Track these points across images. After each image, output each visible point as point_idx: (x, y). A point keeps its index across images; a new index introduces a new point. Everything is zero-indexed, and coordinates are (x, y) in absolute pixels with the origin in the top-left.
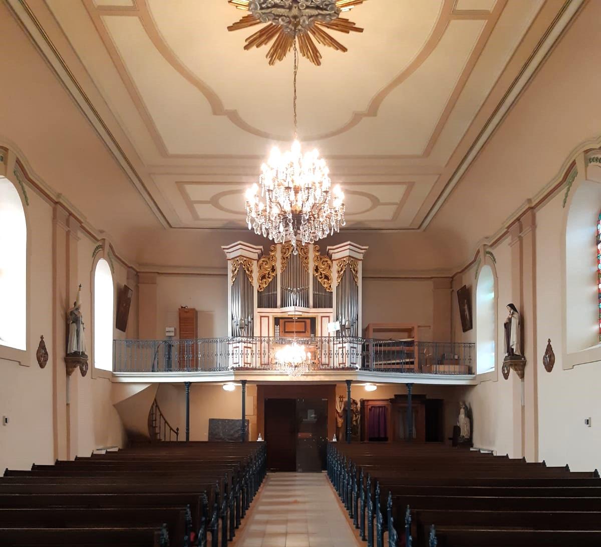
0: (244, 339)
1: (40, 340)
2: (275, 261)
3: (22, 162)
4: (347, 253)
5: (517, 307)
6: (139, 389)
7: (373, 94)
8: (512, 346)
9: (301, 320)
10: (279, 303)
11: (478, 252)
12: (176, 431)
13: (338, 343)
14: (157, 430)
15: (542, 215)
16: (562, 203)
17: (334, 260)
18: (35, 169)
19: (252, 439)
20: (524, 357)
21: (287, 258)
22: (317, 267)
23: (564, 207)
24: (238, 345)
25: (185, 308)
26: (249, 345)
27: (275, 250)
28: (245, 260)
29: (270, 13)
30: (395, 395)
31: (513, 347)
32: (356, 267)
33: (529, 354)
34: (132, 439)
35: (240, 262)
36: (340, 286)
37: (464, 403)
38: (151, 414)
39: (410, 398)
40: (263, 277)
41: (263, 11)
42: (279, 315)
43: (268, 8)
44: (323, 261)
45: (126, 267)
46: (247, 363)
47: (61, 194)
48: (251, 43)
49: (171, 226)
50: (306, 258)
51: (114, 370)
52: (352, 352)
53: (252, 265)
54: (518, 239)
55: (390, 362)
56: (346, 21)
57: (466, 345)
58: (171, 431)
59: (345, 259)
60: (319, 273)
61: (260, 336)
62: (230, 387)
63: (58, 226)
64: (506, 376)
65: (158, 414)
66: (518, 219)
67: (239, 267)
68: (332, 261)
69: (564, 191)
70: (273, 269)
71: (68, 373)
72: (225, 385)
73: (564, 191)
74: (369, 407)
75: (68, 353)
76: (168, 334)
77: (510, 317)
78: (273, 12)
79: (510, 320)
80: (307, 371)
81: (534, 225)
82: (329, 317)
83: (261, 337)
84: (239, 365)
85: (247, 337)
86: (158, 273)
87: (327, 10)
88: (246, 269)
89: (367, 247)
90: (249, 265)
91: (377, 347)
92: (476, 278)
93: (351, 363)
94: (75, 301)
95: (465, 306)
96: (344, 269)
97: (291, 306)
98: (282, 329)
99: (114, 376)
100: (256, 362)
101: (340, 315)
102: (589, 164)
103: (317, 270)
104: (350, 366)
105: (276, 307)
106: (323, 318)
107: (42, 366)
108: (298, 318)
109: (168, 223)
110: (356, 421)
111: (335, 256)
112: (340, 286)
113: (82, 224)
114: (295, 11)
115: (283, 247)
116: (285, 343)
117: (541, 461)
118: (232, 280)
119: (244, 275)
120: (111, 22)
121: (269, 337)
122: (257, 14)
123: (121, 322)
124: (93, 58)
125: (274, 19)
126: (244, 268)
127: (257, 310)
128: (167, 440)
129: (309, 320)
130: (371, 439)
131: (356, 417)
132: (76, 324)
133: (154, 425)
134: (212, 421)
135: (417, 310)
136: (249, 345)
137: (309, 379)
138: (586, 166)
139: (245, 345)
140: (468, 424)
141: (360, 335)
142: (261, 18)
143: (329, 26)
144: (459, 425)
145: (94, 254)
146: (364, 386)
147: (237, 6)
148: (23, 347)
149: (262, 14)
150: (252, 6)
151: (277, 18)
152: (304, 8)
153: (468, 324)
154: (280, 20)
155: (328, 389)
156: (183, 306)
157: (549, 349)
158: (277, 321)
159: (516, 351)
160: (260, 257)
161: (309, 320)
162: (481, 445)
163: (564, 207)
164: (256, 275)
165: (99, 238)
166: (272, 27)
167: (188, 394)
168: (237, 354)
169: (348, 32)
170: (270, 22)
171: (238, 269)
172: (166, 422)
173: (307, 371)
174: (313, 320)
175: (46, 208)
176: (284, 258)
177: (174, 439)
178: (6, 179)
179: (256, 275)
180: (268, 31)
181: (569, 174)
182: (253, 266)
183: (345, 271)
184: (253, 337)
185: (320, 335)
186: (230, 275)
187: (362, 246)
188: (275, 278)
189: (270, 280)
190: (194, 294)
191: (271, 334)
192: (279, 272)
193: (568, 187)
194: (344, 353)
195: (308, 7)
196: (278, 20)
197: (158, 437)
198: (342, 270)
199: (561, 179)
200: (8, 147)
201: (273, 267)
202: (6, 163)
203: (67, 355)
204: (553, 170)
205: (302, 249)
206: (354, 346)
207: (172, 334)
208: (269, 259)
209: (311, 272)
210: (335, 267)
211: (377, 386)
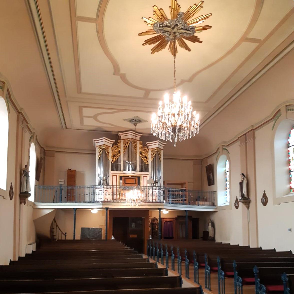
0: (105, 186)
1: (10, 185)
2: (120, 148)
3: (10, 91)
4: (157, 146)
5: (245, 174)
6: (48, 212)
7: (194, 72)
8: (244, 193)
9: (133, 177)
10: (122, 169)
11: (219, 148)
12: (65, 234)
13: (110, 188)
14: (54, 234)
15: (257, 133)
16: (272, 128)
17: (150, 149)
18: (15, 95)
19: (103, 238)
20: (249, 199)
21: (127, 147)
22: (141, 152)
23: (272, 130)
24: (102, 189)
25: (71, 169)
26: (107, 190)
27: (120, 143)
28: (106, 147)
29: (163, 29)
30: (178, 216)
31: (244, 194)
32: (108, 150)
33: (252, 197)
35: (103, 148)
36: (153, 162)
37: (211, 220)
38: (52, 225)
39: (187, 217)
40: (114, 156)
41: (159, 28)
42: (122, 175)
43: (163, 27)
44: (144, 149)
45: (40, 147)
46: (106, 199)
47: (22, 108)
48: (148, 42)
49: (66, 128)
50: (136, 148)
51: (35, 201)
52: (106, 193)
53: (109, 149)
54: (244, 144)
55: (177, 199)
56: (196, 37)
57: (212, 192)
58: (63, 234)
59: (155, 149)
60: (142, 155)
61: (116, 185)
62: (95, 211)
63: (19, 125)
64: (237, 208)
65: (55, 225)
66: (245, 134)
67: (103, 150)
68: (148, 149)
69: (274, 122)
70: (119, 152)
71: (21, 203)
72: (92, 210)
73: (274, 122)
74: (164, 222)
75: (21, 192)
76: (60, 183)
77: (243, 179)
78: (164, 29)
79: (243, 181)
80: (141, 203)
81: (254, 138)
82: (147, 176)
83: (116, 186)
84: (161, 201)
85: (106, 185)
86: (56, 151)
87: (190, 31)
88: (106, 151)
89: (166, 144)
90: (108, 149)
91: (176, 192)
92: (216, 161)
94: (26, 164)
95: (210, 173)
96: (155, 154)
97: (128, 170)
98: (123, 182)
99: (34, 205)
100: (110, 198)
101: (153, 176)
102: (288, 112)
103: (141, 153)
104: (105, 200)
105: (120, 171)
106: (144, 177)
107: (11, 199)
108: (132, 177)
109: (66, 125)
110: (157, 229)
111: (150, 147)
112: (153, 162)
113: (28, 125)
114: (175, 30)
115: (124, 142)
116: (126, 189)
117: (259, 247)
118: (99, 156)
119: (105, 153)
120: (81, 25)
121: (116, 186)
122: (156, 29)
124: (64, 42)
125: (163, 32)
126: (105, 151)
127: (111, 172)
128: (60, 239)
129: (137, 178)
130: (165, 238)
131: (157, 227)
132: (26, 177)
133: (53, 231)
134: (83, 229)
136: (107, 190)
137: (141, 207)
138: (287, 112)
139: (105, 189)
140: (213, 230)
141: (162, 185)
142: (157, 31)
143: (187, 39)
144: (208, 231)
145: (30, 141)
146: (162, 211)
147: (147, 24)
148: (5, 189)
149: (158, 29)
150: (155, 25)
151: (165, 32)
152: (180, 29)
153: (211, 181)
154: (166, 33)
155: (145, 212)
156: (70, 169)
157: (265, 196)
158: (121, 178)
159: (246, 196)
160: (113, 145)
161: (137, 178)
162: (218, 240)
163: (272, 130)
164: (110, 155)
166: (160, 36)
167: (75, 214)
168: (101, 194)
169: (195, 43)
170: (160, 34)
171: (102, 151)
172: (60, 229)
173: (141, 203)
174: (139, 178)
175: (15, 115)
176: (125, 147)
177: (63, 238)
178: (3, 99)
179: (110, 155)
180: (157, 38)
181: (276, 115)
182: (109, 150)
183: (155, 155)
184: (109, 185)
185: (142, 185)
186: (97, 154)
187: (163, 143)
188: (120, 156)
189: (118, 157)
190: (78, 164)
191: (118, 184)
192: (122, 153)
193: (275, 121)
194: (155, 194)
195: (182, 29)
196: (165, 33)
197: (55, 238)
198: (154, 154)
199: (272, 117)
200: (5, 81)
201: (119, 151)
202: (3, 91)
203: (20, 193)
204: (268, 112)
205: (134, 143)
206: (107, 190)
207: (63, 183)
208: (117, 147)
209: (138, 154)
210: (150, 152)
211: (169, 211)
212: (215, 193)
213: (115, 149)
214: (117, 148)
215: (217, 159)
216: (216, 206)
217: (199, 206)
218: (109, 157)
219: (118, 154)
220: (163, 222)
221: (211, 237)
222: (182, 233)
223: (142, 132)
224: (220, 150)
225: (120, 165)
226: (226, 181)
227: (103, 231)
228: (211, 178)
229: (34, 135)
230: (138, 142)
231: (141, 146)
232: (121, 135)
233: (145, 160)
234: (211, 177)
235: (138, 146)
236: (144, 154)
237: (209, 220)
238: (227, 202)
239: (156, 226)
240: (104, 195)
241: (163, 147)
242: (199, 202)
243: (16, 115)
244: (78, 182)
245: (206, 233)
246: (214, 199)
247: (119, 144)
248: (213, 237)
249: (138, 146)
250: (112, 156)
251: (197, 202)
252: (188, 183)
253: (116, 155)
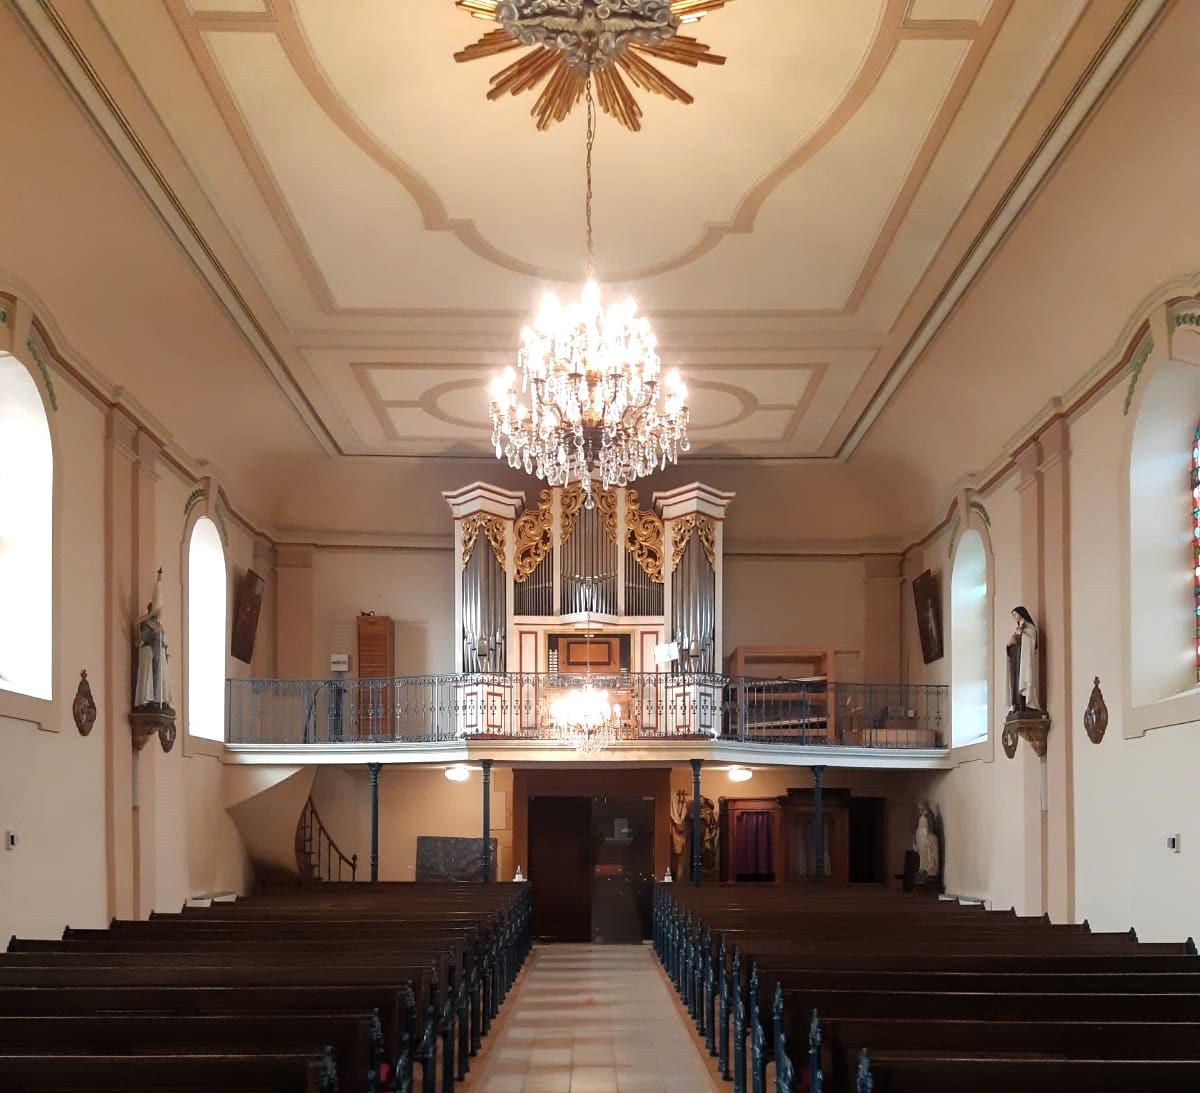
0: (488, 678)
1: (80, 679)
2: (550, 522)
3: (44, 324)
4: (692, 506)
5: (1033, 612)
6: (277, 777)
7: (745, 188)
8: (1022, 691)
9: (602, 639)
10: (557, 605)
11: (955, 503)
12: (352, 862)
13: (675, 684)
14: (314, 860)
15: (1081, 429)
16: (1122, 406)
17: (668, 520)
18: (71, 338)
19: (503, 877)
20: (1047, 714)
21: (573, 515)
22: (633, 533)
23: (1126, 413)
24: (475, 689)
25: (369, 615)
26: (498, 690)
27: (548, 500)
28: (489, 520)
29: (540, 25)
30: (789, 790)
31: (1023, 694)
32: (711, 534)
33: (1055, 708)
35: (479, 523)
36: (679, 571)
37: (927, 805)
38: (302, 827)
39: (819, 795)
40: (526, 554)
41: (526, 22)
42: (558, 630)
43: (535, 15)
44: (646, 522)
45: (252, 534)
46: (493, 726)
47: (122, 388)
48: (502, 85)
49: (340, 452)
50: (611, 516)
51: (229, 739)
52: (703, 703)
53: (504, 529)
54: (1034, 478)
55: (778, 723)
57: (930, 689)
58: (342, 861)
59: (688, 518)
60: (637, 546)
61: (518, 671)
62: (460, 774)
64: (1010, 752)
65: (316, 826)
66: (1035, 438)
67: (477, 533)
68: (663, 522)
69: (1127, 381)
70: (546, 538)
71: (137, 746)
72: (448, 768)
73: (1127, 381)
74: (738, 813)
75: (136, 705)
76: (335, 668)
77: (1019, 633)
78: (545, 24)
79: (1018, 639)
80: (614, 741)
81: (1066, 449)
82: (656, 633)
83: (521, 673)
84: (477, 730)
85: (494, 673)
86: (316, 546)
87: (654, 21)
88: (490, 538)
89: (732, 494)
90: (498, 529)
91: (752, 694)
92: (950, 556)
94: (150, 601)
96: (687, 538)
97: (580, 611)
98: (563, 658)
99: (227, 751)
100: (510, 723)
101: (679, 630)
102: (1177, 328)
103: (632, 539)
104: (700, 730)
105: (551, 613)
106: (645, 636)
107: (84, 730)
108: (596, 636)
109: (336, 445)
110: (712, 841)
111: (668, 513)
112: (679, 571)
113: (165, 448)
114: (588, 23)
117: (1079, 921)
118: (463, 559)
119: (487, 549)
120: (222, 45)
121: (536, 673)
122: (514, 28)
124: (185, 117)
126: (487, 536)
127: (512, 619)
128: (334, 878)
129: (618, 640)
130: (741, 878)
131: (711, 832)
132: (153, 647)
133: (308, 850)
134: (423, 841)
136: (498, 690)
137: (617, 757)
138: (1171, 331)
139: (490, 689)
140: (935, 848)
141: (719, 669)
142: (521, 37)
143: (657, 52)
144: (915, 850)
145: (188, 508)
146: (727, 772)
147: (472, 13)
148: (46, 694)
149: (522, 28)
150: (504, 12)
151: (553, 35)
152: (607, 15)
153: (934, 647)
154: (559, 39)
155: (654, 778)
156: (366, 612)
157: (1097, 698)
158: (553, 641)
159: (1030, 701)
160: (518, 513)
161: (618, 640)
162: (959, 889)
163: (1126, 413)
164: (510, 550)
165: (198, 476)
166: (543, 55)
167: (376, 787)
168: (473, 707)
169: (695, 65)
170: (539, 45)
171: (474, 538)
172: (331, 843)
173: (614, 741)
174: (625, 640)
175: (91, 417)
176: (567, 516)
177: (347, 877)
178: (12, 358)
179: (510, 550)
180: (536, 61)
181: (1136, 348)
182: (505, 532)
183: (688, 542)
184: (505, 673)
185: (638, 670)
186: (459, 549)
187: (724, 491)
188: (549, 555)
189: (539, 559)
190: (386, 588)
191: (542, 668)
192: (557, 543)
193: (1133, 373)
194: (688, 706)
195: (614, 14)
196: (555, 39)
197: (316, 874)
198: (682, 539)
199: (1119, 358)
200: (15, 293)
201: (545, 533)
202: (11, 327)
203: (134, 709)
204: (1105, 339)
205: (603, 497)
206: (708, 692)
207: (344, 668)
208: (537, 517)
209: (621, 543)
210: (669, 534)
211: (753, 772)
227: (499, 848)
229: (207, 486)
240: (697, 711)
243: (102, 417)
244: (401, 664)
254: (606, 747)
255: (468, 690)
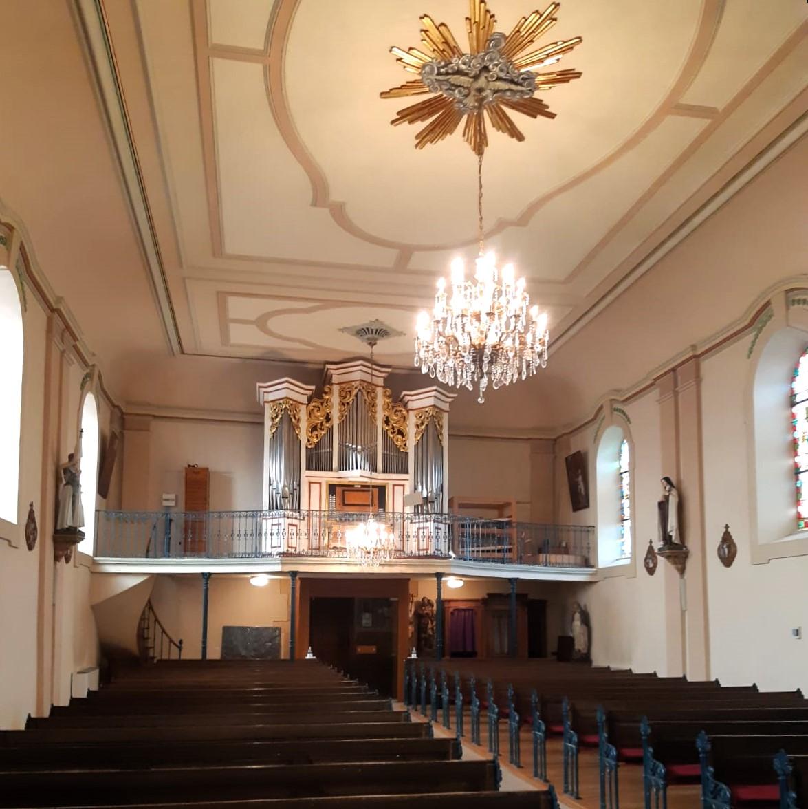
0: (289, 513)
1: (29, 508)
2: (331, 407)
3: (27, 250)
4: (431, 401)
5: (673, 480)
6: (131, 582)
7: (534, 197)
8: (670, 532)
9: (365, 487)
10: (335, 464)
11: (601, 408)
12: (179, 645)
13: (301, 518)
14: (150, 644)
15: (707, 365)
16: (747, 353)
17: (411, 410)
18: (41, 262)
19: (284, 655)
20: (686, 547)
21: (348, 403)
22: (387, 418)
23: (749, 357)
24: (281, 520)
25: (194, 466)
26: (295, 522)
27: (330, 392)
28: (291, 405)
29: (447, 80)
30: (488, 594)
31: (671, 534)
32: (298, 413)
33: (692, 543)
34: (111, 660)
35: (284, 407)
36: (420, 445)
37: (579, 605)
38: (142, 619)
39: (514, 596)
40: (314, 429)
41: (438, 78)
42: (335, 481)
43: (447, 74)
44: (396, 411)
45: (110, 405)
46: (292, 547)
47: (62, 298)
48: (407, 115)
49: (182, 352)
50: (373, 406)
51: (96, 553)
52: (290, 531)
53: (300, 411)
54: (672, 395)
57: (583, 529)
58: (172, 644)
59: (427, 409)
60: (391, 426)
61: (318, 509)
62: (261, 581)
64: (651, 571)
65: (152, 619)
66: (673, 370)
67: (283, 413)
68: (408, 411)
69: (752, 336)
70: (328, 418)
71: (57, 559)
72: (253, 577)
73: (752, 336)
74: (451, 610)
75: (59, 528)
76: (165, 503)
77: (667, 494)
78: (450, 80)
79: (667, 498)
80: (388, 559)
81: (698, 379)
82: (403, 486)
83: (320, 511)
84: (442, 553)
85: (292, 510)
86: (154, 416)
87: (523, 86)
88: (292, 416)
89: (455, 395)
90: (296, 411)
91: (483, 530)
92: (594, 442)
93: (289, 547)
94: (73, 452)
95: (578, 477)
96: (426, 423)
97: (353, 469)
98: (339, 500)
99: (95, 563)
100: (302, 545)
101: (419, 484)
102: (792, 307)
103: (387, 422)
104: (288, 550)
105: (331, 469)
106: (396, 487)
107: (30, 548)
108: (362, 486)
109: (180, 345)
110: (432, 629)
111: (411, 405)
112: (420, 445)
113: (77, 343)
114: (482, 82)
115: (342, 390)
117: (713, 679)
118: (271, 430)
119: (288, 422)
120: (221, 69)
121: (320, 511)
122: (429, 81)
123: (102, 489)
124: (176, 116)
126: (290, 415)
127: (305, 473)
128: (165, 657)
129: (377, 490)
130: (455, 655)
131: (432, 623)
132: (72, 486)
133: (146, 636)
134: (227, 631)
135: (513, 480)
136: (295, 522)
137: (386, 570)
138: (788, 308)
139: (290, 521)
140: (586, 634)
141: (446, 510)
142: (431, 87)
143: (514, 106)
144: (571, 635)
145: (82, 387)
146: (446, 581)
147: (405, 67)
148: (15, 521)
149: (434, 81)
150: (427, 69)
151: (453, 88)
152: (494, 79)
153: (581, 499)
154: (457, 91)
155: (399, 584)
156: (192, 464)
157: (727, 539)
158: (332, 489)
159: (675, 539)
160: (310, 400)
161: (377, 490)
162: (600, 660)
163: (749, 357)
164: (304, 426)
165: (90, 364)
166: (441, 100)
167: (207, 590)
168: (277, 534)
169: (535, 117)
170: (440, 93)
171: (280, 416)
172: (164, 631)
173: (388, 559)
174: (382, 489)
175: (41, 316)
176: (343, 404)
177: (174, 656)
178: (8, 271)
179: (304, 426)
180: (433, 104)
181: (760, 317)
182: (301, 413)
183: (427, 425)
184: (299, 510)
185: (391, 510)
186: (268, 423)
187: (449, 392)
188: (331, 430)
189: (323, 433)
190: (214, 451)
191: (324, 507)
192: (336, 422)
193: (755, 332)
194: (427, 533)
195: (499, 79)
196: (454, 90)
197: (151, 654)
198: (422, 424)
199: (746, 323)
200: (14, 224)
201: (328, 415)
202: (9, 250)
203: (56, 531)
204: (737, 308)
205: (368, 392)
206: (294, 523)
207: (173, 504)
208: (322, 404)
209: (380, 424)
210: (412, 419)
211: (464, 581)
212: (590, 530)
213: (316, 410)
214: (320, 406)
215: (596, 439)
216: (593, 567)
217: (546, 566)
218: (300, 432)
219: (324, 423)
220: (448, 611)
221: (580, 651)
222: (499, 641)
223: (390, 364)
224: (606, 412)
225: (331, 454)
226: (622, 497)
227: (283, 634)
228: (581, 490)
230: (380, 391)
231: (387, 400)
232: (332, 372)
233: (397, 440)
234: (579, 487)
235: (381, 401)
236: (395, 425)
237: (576, 606)
238: (624, 557)
239: (430, 622)
241: (448, 405)
242: (548, 555)
245: (567, 642)
246: (589, 548)
247: (327, 397)
248: (585, 651)
249: (381, 401)
250: (307, 431)
251: (542, 557)
252: (518, 503)
253: (319, 426)
254: (382, 563)
255: (275, 521)
